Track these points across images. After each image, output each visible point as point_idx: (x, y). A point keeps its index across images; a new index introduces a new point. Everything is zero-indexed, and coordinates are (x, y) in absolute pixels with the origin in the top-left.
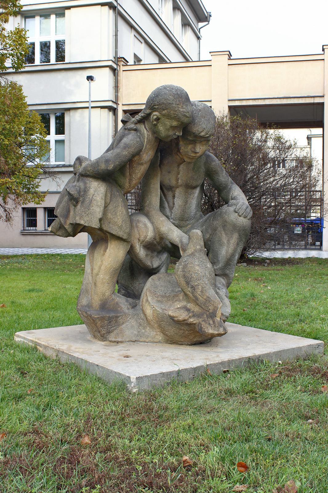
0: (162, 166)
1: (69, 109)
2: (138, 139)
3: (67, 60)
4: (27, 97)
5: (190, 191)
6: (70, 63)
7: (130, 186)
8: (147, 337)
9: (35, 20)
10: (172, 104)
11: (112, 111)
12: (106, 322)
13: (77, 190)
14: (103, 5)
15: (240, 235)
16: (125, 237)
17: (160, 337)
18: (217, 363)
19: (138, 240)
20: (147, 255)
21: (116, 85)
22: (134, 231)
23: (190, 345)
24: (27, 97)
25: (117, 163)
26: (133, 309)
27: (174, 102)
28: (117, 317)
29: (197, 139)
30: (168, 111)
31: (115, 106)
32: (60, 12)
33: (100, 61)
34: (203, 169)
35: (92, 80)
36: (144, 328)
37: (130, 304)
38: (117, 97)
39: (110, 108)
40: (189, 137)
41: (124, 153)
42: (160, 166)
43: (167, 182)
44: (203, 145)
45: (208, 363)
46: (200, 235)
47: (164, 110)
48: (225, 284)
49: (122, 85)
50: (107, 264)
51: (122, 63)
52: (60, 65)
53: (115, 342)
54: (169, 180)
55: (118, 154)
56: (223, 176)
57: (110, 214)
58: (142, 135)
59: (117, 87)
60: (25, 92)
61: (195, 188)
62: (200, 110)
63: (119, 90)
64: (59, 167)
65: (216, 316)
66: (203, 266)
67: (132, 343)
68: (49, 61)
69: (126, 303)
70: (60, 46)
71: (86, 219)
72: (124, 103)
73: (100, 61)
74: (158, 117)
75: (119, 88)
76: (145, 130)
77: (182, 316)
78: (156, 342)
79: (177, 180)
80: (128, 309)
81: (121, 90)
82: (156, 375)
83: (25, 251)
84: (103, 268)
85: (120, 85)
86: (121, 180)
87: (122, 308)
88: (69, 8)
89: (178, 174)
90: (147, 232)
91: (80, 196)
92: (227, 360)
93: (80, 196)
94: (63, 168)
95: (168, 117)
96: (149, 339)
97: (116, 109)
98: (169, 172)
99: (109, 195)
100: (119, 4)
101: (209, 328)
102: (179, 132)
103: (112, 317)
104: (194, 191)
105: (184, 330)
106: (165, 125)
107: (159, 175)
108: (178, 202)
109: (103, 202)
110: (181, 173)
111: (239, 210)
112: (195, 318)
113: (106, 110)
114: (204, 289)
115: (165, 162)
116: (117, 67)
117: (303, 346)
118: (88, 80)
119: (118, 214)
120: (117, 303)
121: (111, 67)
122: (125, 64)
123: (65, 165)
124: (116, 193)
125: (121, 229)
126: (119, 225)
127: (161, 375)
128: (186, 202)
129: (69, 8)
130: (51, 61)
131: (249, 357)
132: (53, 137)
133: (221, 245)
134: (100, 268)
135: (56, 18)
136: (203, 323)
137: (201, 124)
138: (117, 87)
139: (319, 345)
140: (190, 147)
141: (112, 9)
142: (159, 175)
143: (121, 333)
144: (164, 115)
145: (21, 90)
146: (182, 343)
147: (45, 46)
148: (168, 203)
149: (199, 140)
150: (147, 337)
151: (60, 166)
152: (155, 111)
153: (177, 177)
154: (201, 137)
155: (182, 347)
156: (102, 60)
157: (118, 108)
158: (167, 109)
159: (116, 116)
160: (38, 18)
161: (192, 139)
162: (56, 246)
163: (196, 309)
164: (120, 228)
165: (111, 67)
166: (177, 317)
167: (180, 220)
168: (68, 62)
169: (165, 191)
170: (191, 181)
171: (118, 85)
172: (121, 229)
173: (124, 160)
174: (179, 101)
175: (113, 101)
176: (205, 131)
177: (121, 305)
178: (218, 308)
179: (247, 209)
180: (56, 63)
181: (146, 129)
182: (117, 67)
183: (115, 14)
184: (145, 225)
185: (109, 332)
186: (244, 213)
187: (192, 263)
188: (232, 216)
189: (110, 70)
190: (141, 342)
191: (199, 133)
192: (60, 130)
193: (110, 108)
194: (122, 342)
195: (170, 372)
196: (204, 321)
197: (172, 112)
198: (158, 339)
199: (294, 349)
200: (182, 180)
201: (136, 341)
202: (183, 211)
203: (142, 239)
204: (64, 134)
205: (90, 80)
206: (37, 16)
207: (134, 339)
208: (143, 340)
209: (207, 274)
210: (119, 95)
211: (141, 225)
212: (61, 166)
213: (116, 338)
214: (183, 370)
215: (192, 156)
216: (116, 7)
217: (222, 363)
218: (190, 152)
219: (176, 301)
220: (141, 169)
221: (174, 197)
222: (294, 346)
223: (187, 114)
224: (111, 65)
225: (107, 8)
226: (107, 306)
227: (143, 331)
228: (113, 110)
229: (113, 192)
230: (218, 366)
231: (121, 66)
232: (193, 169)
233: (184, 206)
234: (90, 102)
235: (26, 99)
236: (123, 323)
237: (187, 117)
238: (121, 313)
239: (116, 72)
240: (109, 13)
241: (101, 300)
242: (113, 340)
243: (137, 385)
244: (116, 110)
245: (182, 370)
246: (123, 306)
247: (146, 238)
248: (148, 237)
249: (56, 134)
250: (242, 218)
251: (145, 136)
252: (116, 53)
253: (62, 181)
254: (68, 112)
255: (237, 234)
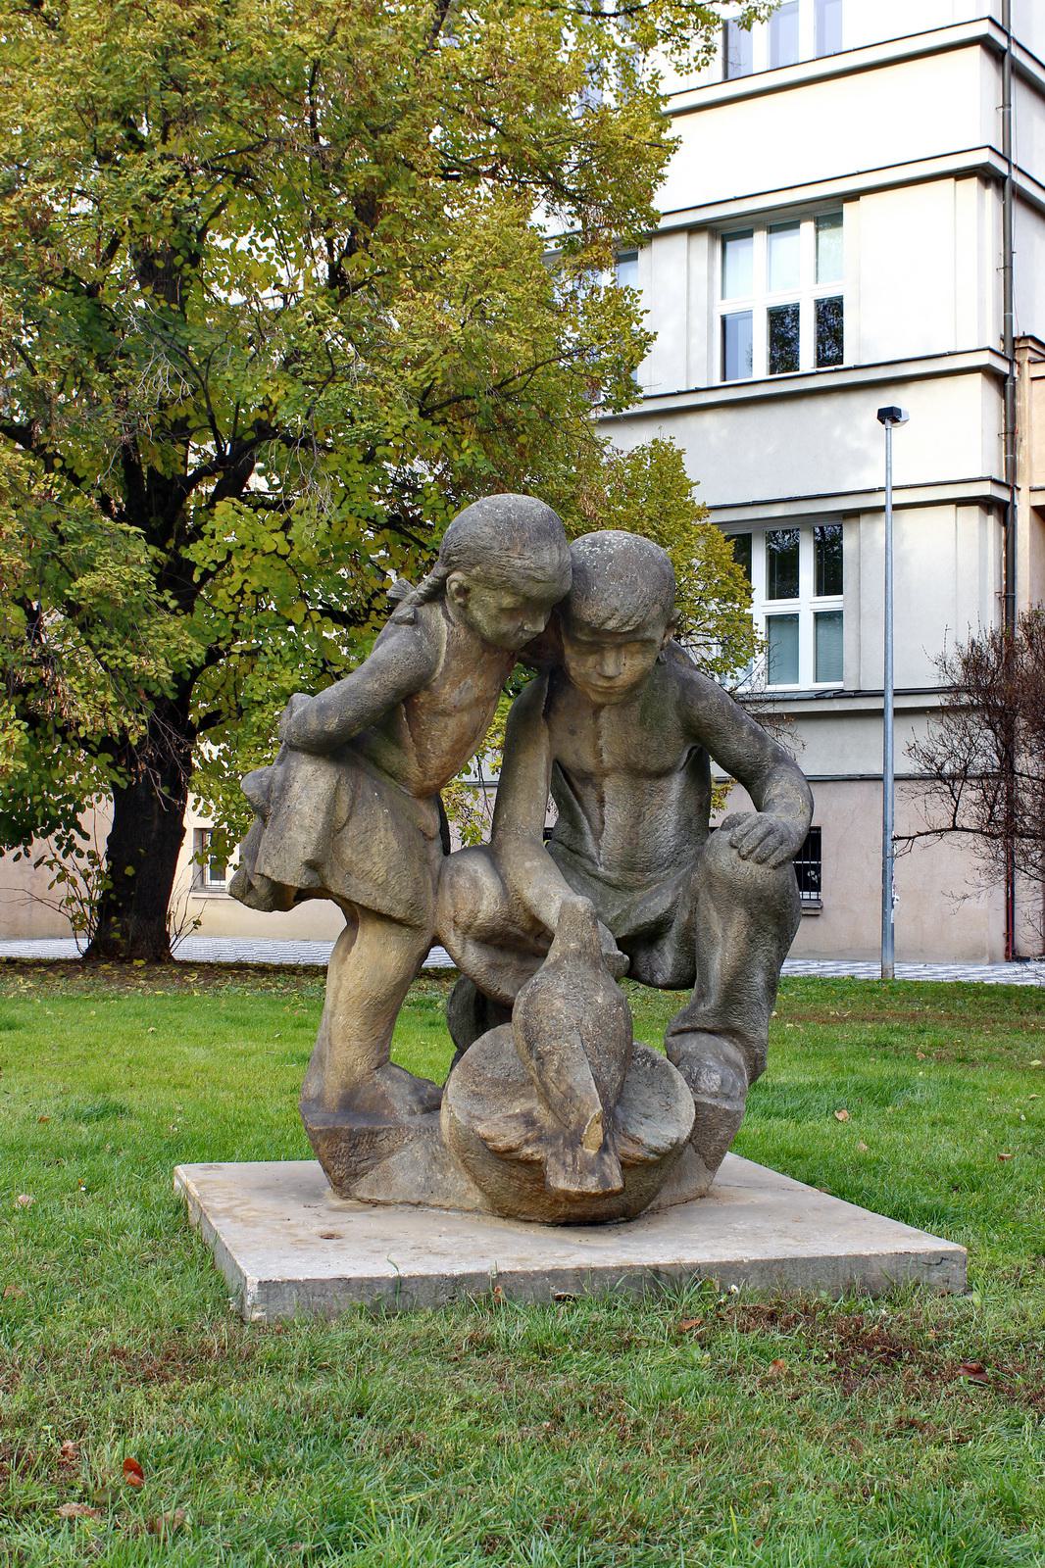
0: (552, 715)
1: (855, 514)
2: (412, 648)
3: (848, 362)
4: (698, 483)
5: (647, 784)
6: (856, 368)
7: (424, 773)
8: (447, 1195)
9: (636, 267)
10: (492, 548)
11: (995, 511)
12: (343, 1144)
13: (261, 786)
14: (960, 175)
15: (752, 915)
16: (399, 912)
17: (476, 1198)
18: (534, 1272)
19: (452, 923)
20: (493, 967)
21: (1009, 426)
22: (443, 898)
23: (543, 1223)
24: (698, 483)
25: (350, 713)
26: (425, 1116)
27: (495, 544)
28: (374, 1134)
29: (600, 640)
30: (484, 567)
31: (1005, 496)
32: (827, 212)
33: (951, 354)
34: (672, 722)
35: (895, 420)
36: (443, 1168)
37: (421, 1101)
38: (1012, 467)
39: (987, 504)
40: (579, 636)
41: (368, 687)
42: (546, 715)
43: (570, 759)
44: (632, 655)
45: (502, 1269)
46: (582, 910)
47: (473, 566)
48: (742, 1062)
49: (1030, 427)
50: (351, 986)
51: (1030, 354)
52: (827, 375)
53: (369, 1202)
54: (576, 753)
55: (351, 690)
56: (740, 739)
57: (349, 851)
58: (433, 637)
59: (1011, 436)
60: (691, 469)
61: (664, 773)
62: (611, 558)
63: (1018, 441)
64: (824, 698)
65: (581, 1143)
66: (578, 1000)
67: (410, 1208)
68: (793, 365)
69: (409, 1098)
70: (830, 312)
71: (275, 862)
72: (1036, 485)
73: (951, 354)
74: (460, 586)
75: (1018, 436)
76: (443, 621)
77: (509, 1136)
78: (468, 1211)
79: (598, 753)
80: (412, 1113)
81: (1025, 442)
82: (323, 1282)
83: (831, 969)
84: (342, 996)
85: (1022, 428)
86: (392, 758)
87: (393, 1109)
88: (854, 196)
89: (598, 736)
90: (477, 902)
91: (268, 801)
92: (574, 1267)
93: (268, 801)
94: (835, 701)
95: (486, 581)
96: (452, 1201)
97: (1007, 503)
98: (573, 732)
99: (345, 798)
100: (1015, 166)
101: (559, 1176)
102: (534, 622)
103: (361, 1134)
104: (663, 783)
105: (519, 1179)
106: (484, 606)
107: (544, 739)
108: (615, 816)
109: (320, 818)
110: (604, 733)
111: (741, 840)
112: (541, 1147)
113: (976, 509)
114: (566, 1063)
115: (561, 704)
116: (1012, 370)
117: (876, 1256)
118: (883, 423)
119: (374, 850)
120: (383, 1096)
121: (987, 371)
122: (1040, 358)
123: (842, 691)
124: (369, 793)
125: (385, 891)
126: (380, 881)
127: (341, 1285)
128: (638, 818)
129: (854, 196)
130: (801, 367)
131: (657, 1266)
132: (807, 602)
133: (712, 943)
134: (336, 997)
135: (817, 230)
136: (552, 1160)
137: (605, 596)
138: (1011, 436)
139: (942, 1259)
140: (591, 660)
141: (993, 185)
142: (544, 739)
143: (385, 1178)
144: (477, 580)
145: (679, 464)
146: (528, 1218)
147: (782, 320)
148: (589, 820)
149: (608, 640)
150: (447, 1195)
151: (827, 695)
152: (455, 570)
153: (595, 745)
154: (613, 633)
155: (520, 1229)
156: (959, 350)
157: (1016, 503)
158: (479, 563)
159: (1010, 528)
160: (760, 237)
161: (590, 639)
162: (814, 952)
163: (547, 1120)
164: (383, 887)
165: (987, 371)
166: (493, 1140)
167: (623, 869)
168: (852, 365)
169: (578, 786)
170: (642, 756)
171: (1014, 428)
172: (385, 891)
173: (369, 703)
174: (510, 539)
175: (995, 482)
176: (617, 616)
177: (392, 1101)
178: (587, 1120)
179: (770, 838)
180: (814, 371)
181: (448, 618)
182: (1012, 370)
183: (1004, 199)
184: (475, 883)
185: (355, 1175)
186: (756, 847)
187: (548, 990)
188: (722, 858)
189: (986, 382)
190: (433, 1207)
191: (603, 624)
192: (830, 580)
193: (987, 504)
194: (386, 1204)
195: (371, 1279)
196: (554, 1154)
197: (493, 570)
198: (472, 1201)
199: (837, 1258)
200: (611, 753)
201: (419, 1203)
202: (630, 844)
203: (463, 918)
204: (840, 592)
205: (888, 422)
206: (760, 229)
207: (415, 1197)
208: (438, 1203)
209: (588, 1022)
210: (1021, 457)
211: (462, 881)
212: (831, 694)
213: (371, 1191)
214: (413, 1280)
215: (602, 687)
216: (1005, 178)
217: (555, 1275)
218: (595, 675)
219: (522, 1095)
220: (446, 727)
221: (601, 801)
222: (841, 1250)
223: (539, 575)
224: (988, 365)
225: (973, 183)
226: (357, 1102)
227: (439, 1177)
228: (1000, 510)
229: (360, 792)
230: (538, 1283)
231: (1026, 364)
232: (642, 721)
233: (632, 827)
234: (889, 489)
235: (696, 491)
236: (391, 1152)
237: (539, 581)
238: (386, 1123)
239: (1009, 384)
240: (981, 199)
241: (345, 1086)
242: (367, 1196)
243: (262, 1302)
244: (1010, 508)
245: (410, 1277)
246: (397, 1105)
247: (475, 918)
248: (481, 916)
249: (771, 597)
250: (749, 864)
251: (440, 638)
252: (1008, 323)
253: (800, 745)
254: (853, 521)
255: (742, 911)
